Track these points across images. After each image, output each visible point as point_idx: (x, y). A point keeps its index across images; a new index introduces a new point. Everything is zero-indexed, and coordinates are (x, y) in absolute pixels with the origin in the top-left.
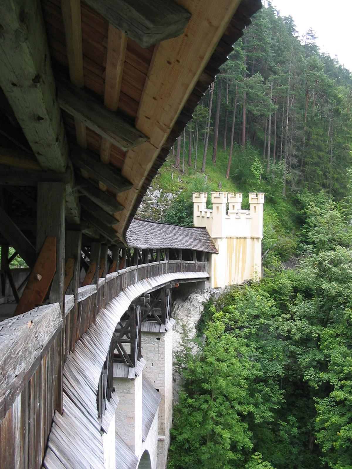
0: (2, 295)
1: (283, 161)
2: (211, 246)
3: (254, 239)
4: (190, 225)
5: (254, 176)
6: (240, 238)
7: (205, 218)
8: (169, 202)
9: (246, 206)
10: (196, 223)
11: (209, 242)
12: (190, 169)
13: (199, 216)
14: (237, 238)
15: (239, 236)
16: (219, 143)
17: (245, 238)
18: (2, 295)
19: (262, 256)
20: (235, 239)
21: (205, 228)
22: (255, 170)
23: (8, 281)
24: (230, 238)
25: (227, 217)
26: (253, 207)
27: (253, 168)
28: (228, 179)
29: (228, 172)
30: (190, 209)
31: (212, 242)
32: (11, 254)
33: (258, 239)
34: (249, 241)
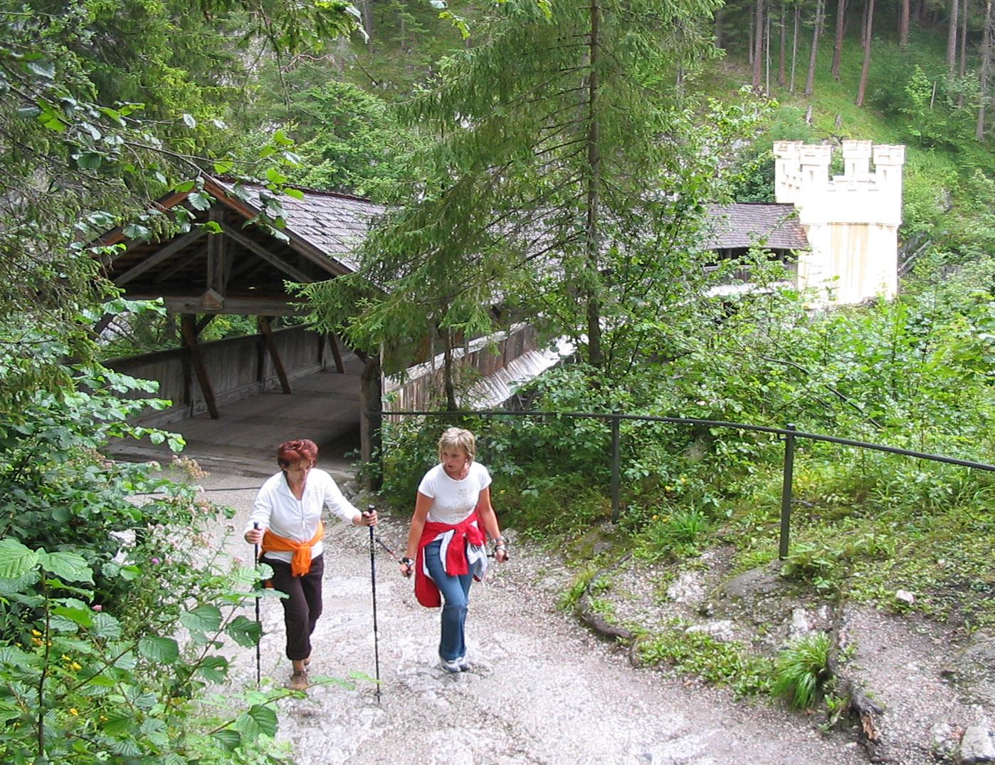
0: (258, 380)
1: (972, 75)
2: (799, 238)
3: (882, 226)
4: (768, 200)
5: (912, 103)
6: (856, 224)
7: (794, 188)
8: (735, 155)
9: (837, 169)
10: (782, 195)
11: (796, 230)
12: (781, 91)
13: (784, 183)
14: (850, 224)
15: (852, 221)
16: (846, 36)
17: (866, 224)
18: (258, 380)
19: (899, 266)
20: (846, 228)
21: (792, 204)
22: (914, 92)
23: (194, 378)
24: (837, 224)
25: (831, 187)
26: (809, 173)
27: (911, 87)
28: (862, 106)
29: (861, 94)
30: (768, 170)
31: (803, 231)
32: (137, 305)
33: (890, 227)
34: (873, 229)
